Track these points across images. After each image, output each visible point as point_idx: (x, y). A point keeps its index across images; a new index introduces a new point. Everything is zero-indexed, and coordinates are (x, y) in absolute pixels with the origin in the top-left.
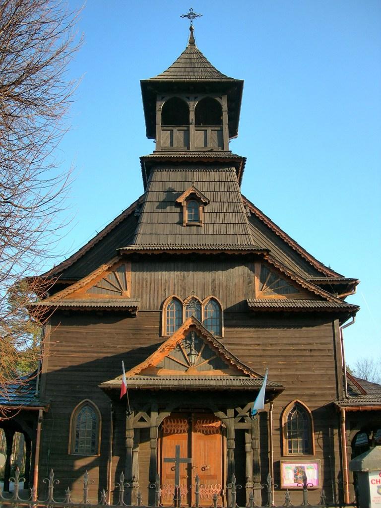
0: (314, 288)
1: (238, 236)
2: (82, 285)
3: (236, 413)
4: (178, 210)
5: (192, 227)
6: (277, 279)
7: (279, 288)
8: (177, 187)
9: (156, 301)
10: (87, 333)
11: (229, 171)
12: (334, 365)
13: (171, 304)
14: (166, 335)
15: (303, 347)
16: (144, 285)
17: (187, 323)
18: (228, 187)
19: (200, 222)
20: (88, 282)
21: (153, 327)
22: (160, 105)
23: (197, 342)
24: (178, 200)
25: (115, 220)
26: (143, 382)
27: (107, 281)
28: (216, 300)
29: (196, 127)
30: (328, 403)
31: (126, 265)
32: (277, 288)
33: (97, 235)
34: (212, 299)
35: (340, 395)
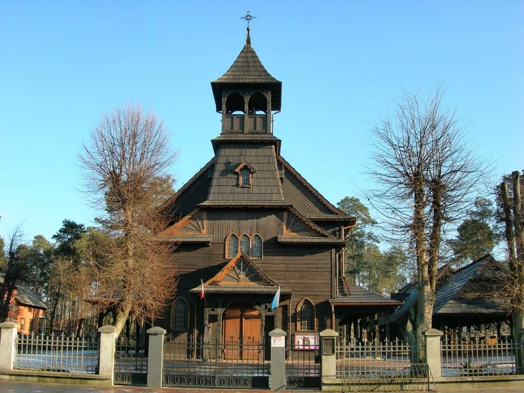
3: (266, 306)
4: (236, 177)
12: (330, 277)
14: (228, 258)
15: (312, 266)
16: (215, 227)
19: (250, 185)
22: (224, 100)
23: (244, 265)
24: (236, 171)
26: (213, 289)
28: (258, 236)
30: (325, 300)
34: (256, 235)
35: (333, 295)
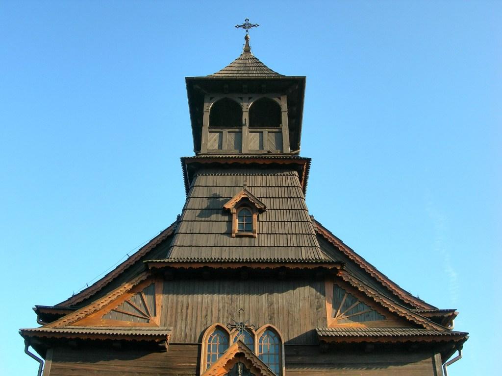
0: (404, 312)
1: (303, 248)
2: (97, 308)
4: (226, 218)
5: (244, 239)
6: (356, 302)
7: (358, 314)
8: (224, 193)
9: (193, 330)
10: (98, 371)
11: (290, 175)
13: (213, 334)
16: (179, 311)
17: (234, 349)
18: (289, 192)
20: (104, 304)
21: (188, 364)
22: (208, 106)
24: (227, 206)
25: (151, 242)
27: (130, 304)
29: (249, 128)
31: (156, 284)
32: (355, 314)
33: (128, 259)
34: (269, 328)
